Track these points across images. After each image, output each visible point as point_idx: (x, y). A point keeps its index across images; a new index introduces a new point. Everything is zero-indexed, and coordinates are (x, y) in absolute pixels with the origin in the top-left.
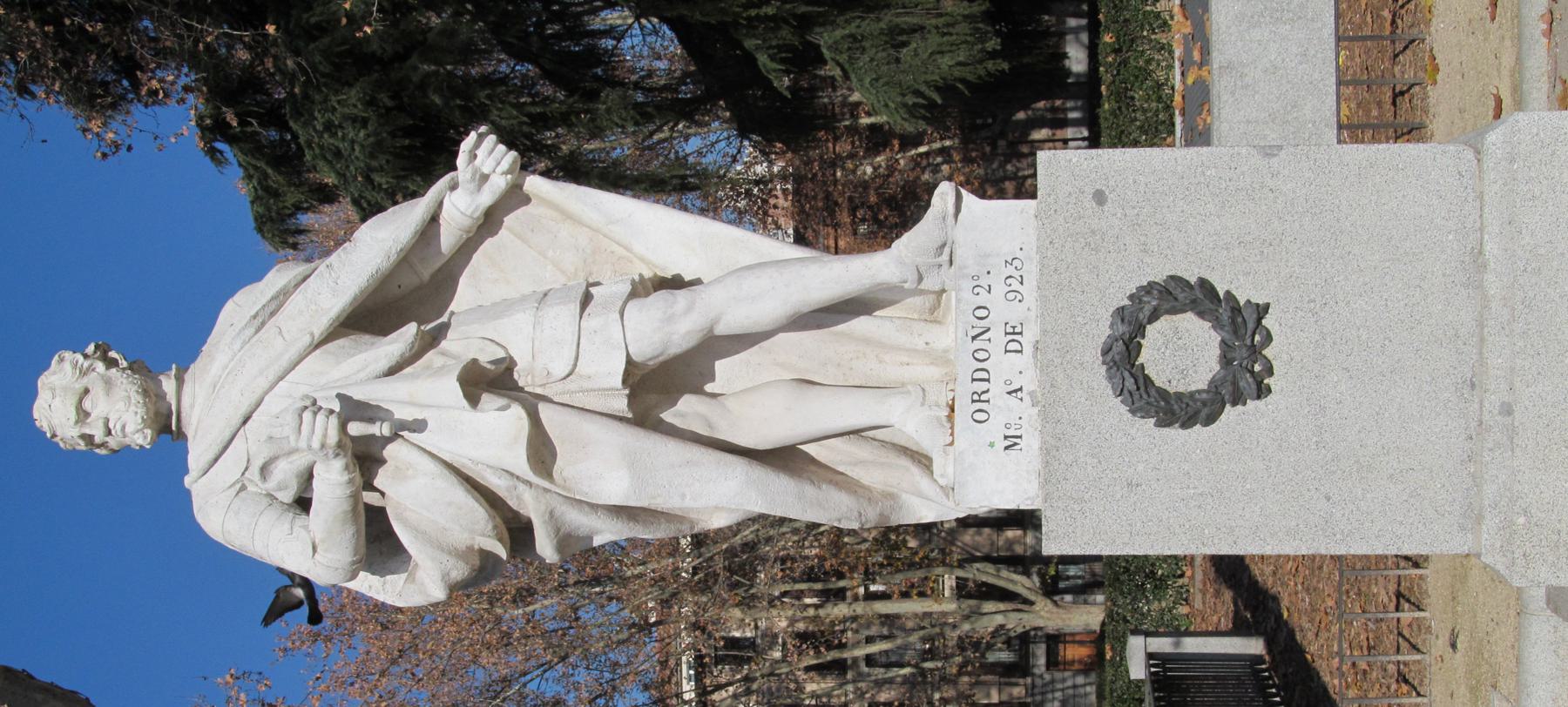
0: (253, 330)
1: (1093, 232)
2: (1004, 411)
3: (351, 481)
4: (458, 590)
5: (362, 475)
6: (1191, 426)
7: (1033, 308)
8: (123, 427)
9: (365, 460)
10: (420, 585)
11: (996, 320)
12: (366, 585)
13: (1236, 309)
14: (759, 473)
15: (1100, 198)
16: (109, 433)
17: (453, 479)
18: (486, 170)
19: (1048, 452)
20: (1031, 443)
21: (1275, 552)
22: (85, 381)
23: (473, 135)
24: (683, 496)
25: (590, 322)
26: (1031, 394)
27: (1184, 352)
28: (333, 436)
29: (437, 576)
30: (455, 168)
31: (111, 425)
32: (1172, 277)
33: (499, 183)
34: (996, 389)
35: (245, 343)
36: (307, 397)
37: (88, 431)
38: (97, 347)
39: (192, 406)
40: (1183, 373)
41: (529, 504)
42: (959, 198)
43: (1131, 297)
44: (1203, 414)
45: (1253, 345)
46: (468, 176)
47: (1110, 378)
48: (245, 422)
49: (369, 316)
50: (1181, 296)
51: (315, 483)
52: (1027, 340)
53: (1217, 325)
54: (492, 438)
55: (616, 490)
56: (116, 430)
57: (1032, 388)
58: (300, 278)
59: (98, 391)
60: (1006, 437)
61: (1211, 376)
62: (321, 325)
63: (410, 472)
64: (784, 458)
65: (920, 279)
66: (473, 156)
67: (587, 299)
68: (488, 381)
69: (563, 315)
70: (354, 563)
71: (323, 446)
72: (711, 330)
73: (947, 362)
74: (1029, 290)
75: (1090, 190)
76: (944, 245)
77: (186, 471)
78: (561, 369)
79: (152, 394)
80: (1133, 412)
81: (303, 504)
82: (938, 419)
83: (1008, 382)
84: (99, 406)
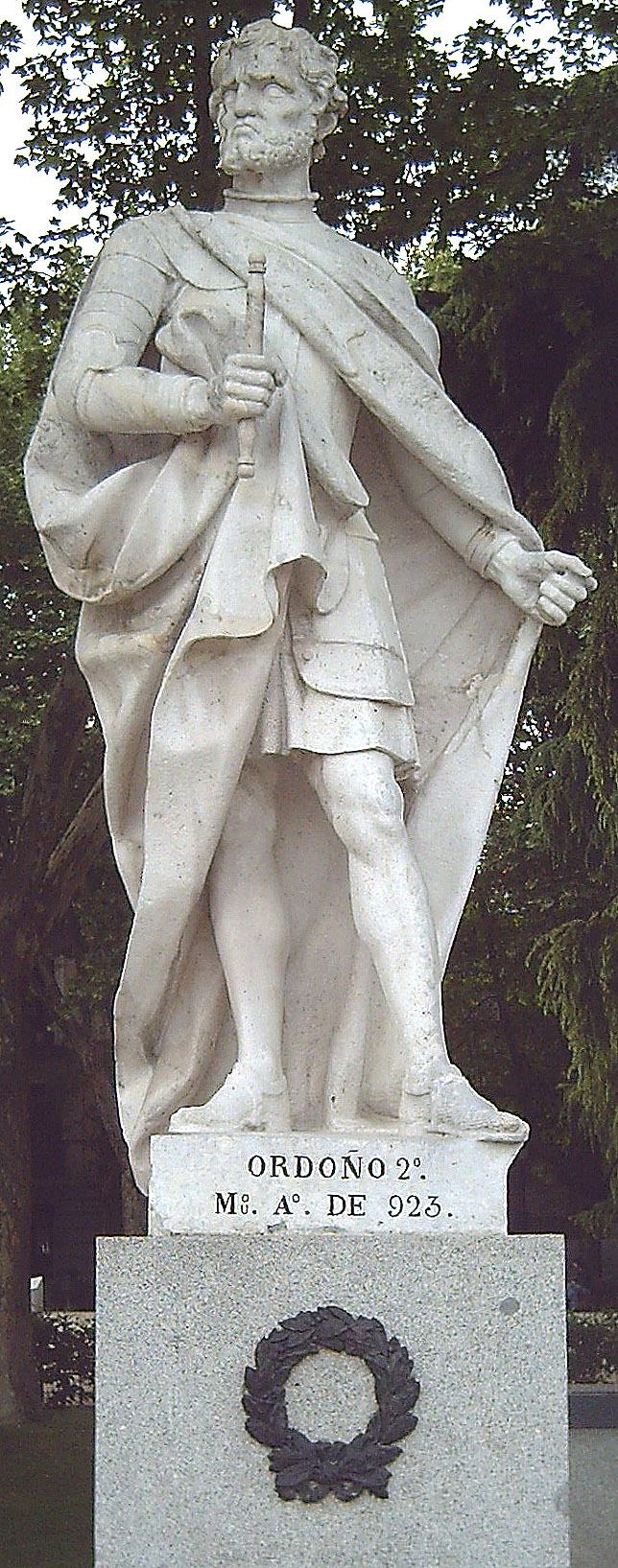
0: (360, 298)
2: (264, 1193)
11: (364, 1185)
14: (185, 905)
15: (509, 1307)
26: (283, 1225)
27: (331, 1401)
31: (247, 120)
34: (288, 1185)
49: (372, 438)
52: (344, 1221)
54: (233, 596)
59: (289, 104)
60: (232, 1195)
68: (299, 586)
74: (404, 1224)
79: (283, 168)
81: (150, 357)
82: (248, 1113)
83: (296, 1198)
84: (275, 103)
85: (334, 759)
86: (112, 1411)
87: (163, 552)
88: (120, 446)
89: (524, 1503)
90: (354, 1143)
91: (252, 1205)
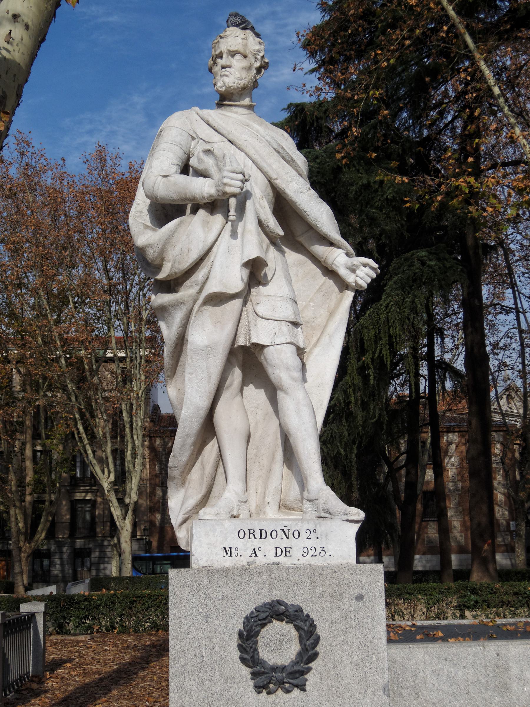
0: (276, 147)
1: (341, 594)
2: (244, 547)
3: (204, 198)
4: (141, 252)
5: (205, 204)
6: (239, 649)
7: (299, 562)
8: (226, 76)
9: (215, 205)
10: (141, 229)
11: (292, 542)
12: (139, 202)
13: (303, 673)
14: (203, 413)
15: (360, 598)
16: (223, 67)
17: (203, 252)
18: (358, 272)
19: (225, 571)
20: (228, 562)
21: (170, 699)
22: (250, 56)
23: (376, 266)
24: (191, 374)
25: (285, 328)
26: (254, 562)
27: (279, 645)
28: (229, 190)
29: (151, 241)
30: (358, 255)
31: (227, 69)
32: (319, 638)
33: (351, 279)
34: (256, 543)
35: (269, 143)
36: (250, 177)
37: (224, 56)
38: (267, 63)
39: (236, 113)
40: (267, 645)
41: (186, 292)
42: (356, 522)
43: (308, 616)
44: (246, 656)
45: (284, 683)
46: (355, 263)
47: (265, 604)
48: (230, 141)
49: (282, 206)
50: (308, 642)
51: (201, 179)
52: (282, 559)
53: (295, 663)
54: (226, 273)
55: (197, 337)
56: (226, 71)
57: (257, 562)
58: (301, 172)
59: (245, 63)
60: (230, 548)
61: (267, 660)
62: (281, 184)
63: (207, 229)
64: (209, 428)
65: (309, 501)
66: (365, 265)
67: (296, 324)
69: (287, 311)
70: (156, 198)
71: (225, 184)
72: (282, 390)
73: (258, 513)
74: (308, 560)
75: (363, 592)
76: (330, 513)
77: (202, 107)
78: (260, 310)
80: (247, 618)
81: (185, 169)
82: (232, 510)
83: (260, 549)
84: (237, 62)
85: (271, 348)
86: (177, 652)
87: (194, 256)
88: (166, 211)
89: (369, 691)
90: (285, 523)
91: (240, 552)
